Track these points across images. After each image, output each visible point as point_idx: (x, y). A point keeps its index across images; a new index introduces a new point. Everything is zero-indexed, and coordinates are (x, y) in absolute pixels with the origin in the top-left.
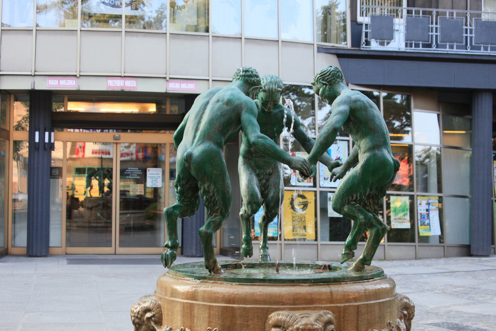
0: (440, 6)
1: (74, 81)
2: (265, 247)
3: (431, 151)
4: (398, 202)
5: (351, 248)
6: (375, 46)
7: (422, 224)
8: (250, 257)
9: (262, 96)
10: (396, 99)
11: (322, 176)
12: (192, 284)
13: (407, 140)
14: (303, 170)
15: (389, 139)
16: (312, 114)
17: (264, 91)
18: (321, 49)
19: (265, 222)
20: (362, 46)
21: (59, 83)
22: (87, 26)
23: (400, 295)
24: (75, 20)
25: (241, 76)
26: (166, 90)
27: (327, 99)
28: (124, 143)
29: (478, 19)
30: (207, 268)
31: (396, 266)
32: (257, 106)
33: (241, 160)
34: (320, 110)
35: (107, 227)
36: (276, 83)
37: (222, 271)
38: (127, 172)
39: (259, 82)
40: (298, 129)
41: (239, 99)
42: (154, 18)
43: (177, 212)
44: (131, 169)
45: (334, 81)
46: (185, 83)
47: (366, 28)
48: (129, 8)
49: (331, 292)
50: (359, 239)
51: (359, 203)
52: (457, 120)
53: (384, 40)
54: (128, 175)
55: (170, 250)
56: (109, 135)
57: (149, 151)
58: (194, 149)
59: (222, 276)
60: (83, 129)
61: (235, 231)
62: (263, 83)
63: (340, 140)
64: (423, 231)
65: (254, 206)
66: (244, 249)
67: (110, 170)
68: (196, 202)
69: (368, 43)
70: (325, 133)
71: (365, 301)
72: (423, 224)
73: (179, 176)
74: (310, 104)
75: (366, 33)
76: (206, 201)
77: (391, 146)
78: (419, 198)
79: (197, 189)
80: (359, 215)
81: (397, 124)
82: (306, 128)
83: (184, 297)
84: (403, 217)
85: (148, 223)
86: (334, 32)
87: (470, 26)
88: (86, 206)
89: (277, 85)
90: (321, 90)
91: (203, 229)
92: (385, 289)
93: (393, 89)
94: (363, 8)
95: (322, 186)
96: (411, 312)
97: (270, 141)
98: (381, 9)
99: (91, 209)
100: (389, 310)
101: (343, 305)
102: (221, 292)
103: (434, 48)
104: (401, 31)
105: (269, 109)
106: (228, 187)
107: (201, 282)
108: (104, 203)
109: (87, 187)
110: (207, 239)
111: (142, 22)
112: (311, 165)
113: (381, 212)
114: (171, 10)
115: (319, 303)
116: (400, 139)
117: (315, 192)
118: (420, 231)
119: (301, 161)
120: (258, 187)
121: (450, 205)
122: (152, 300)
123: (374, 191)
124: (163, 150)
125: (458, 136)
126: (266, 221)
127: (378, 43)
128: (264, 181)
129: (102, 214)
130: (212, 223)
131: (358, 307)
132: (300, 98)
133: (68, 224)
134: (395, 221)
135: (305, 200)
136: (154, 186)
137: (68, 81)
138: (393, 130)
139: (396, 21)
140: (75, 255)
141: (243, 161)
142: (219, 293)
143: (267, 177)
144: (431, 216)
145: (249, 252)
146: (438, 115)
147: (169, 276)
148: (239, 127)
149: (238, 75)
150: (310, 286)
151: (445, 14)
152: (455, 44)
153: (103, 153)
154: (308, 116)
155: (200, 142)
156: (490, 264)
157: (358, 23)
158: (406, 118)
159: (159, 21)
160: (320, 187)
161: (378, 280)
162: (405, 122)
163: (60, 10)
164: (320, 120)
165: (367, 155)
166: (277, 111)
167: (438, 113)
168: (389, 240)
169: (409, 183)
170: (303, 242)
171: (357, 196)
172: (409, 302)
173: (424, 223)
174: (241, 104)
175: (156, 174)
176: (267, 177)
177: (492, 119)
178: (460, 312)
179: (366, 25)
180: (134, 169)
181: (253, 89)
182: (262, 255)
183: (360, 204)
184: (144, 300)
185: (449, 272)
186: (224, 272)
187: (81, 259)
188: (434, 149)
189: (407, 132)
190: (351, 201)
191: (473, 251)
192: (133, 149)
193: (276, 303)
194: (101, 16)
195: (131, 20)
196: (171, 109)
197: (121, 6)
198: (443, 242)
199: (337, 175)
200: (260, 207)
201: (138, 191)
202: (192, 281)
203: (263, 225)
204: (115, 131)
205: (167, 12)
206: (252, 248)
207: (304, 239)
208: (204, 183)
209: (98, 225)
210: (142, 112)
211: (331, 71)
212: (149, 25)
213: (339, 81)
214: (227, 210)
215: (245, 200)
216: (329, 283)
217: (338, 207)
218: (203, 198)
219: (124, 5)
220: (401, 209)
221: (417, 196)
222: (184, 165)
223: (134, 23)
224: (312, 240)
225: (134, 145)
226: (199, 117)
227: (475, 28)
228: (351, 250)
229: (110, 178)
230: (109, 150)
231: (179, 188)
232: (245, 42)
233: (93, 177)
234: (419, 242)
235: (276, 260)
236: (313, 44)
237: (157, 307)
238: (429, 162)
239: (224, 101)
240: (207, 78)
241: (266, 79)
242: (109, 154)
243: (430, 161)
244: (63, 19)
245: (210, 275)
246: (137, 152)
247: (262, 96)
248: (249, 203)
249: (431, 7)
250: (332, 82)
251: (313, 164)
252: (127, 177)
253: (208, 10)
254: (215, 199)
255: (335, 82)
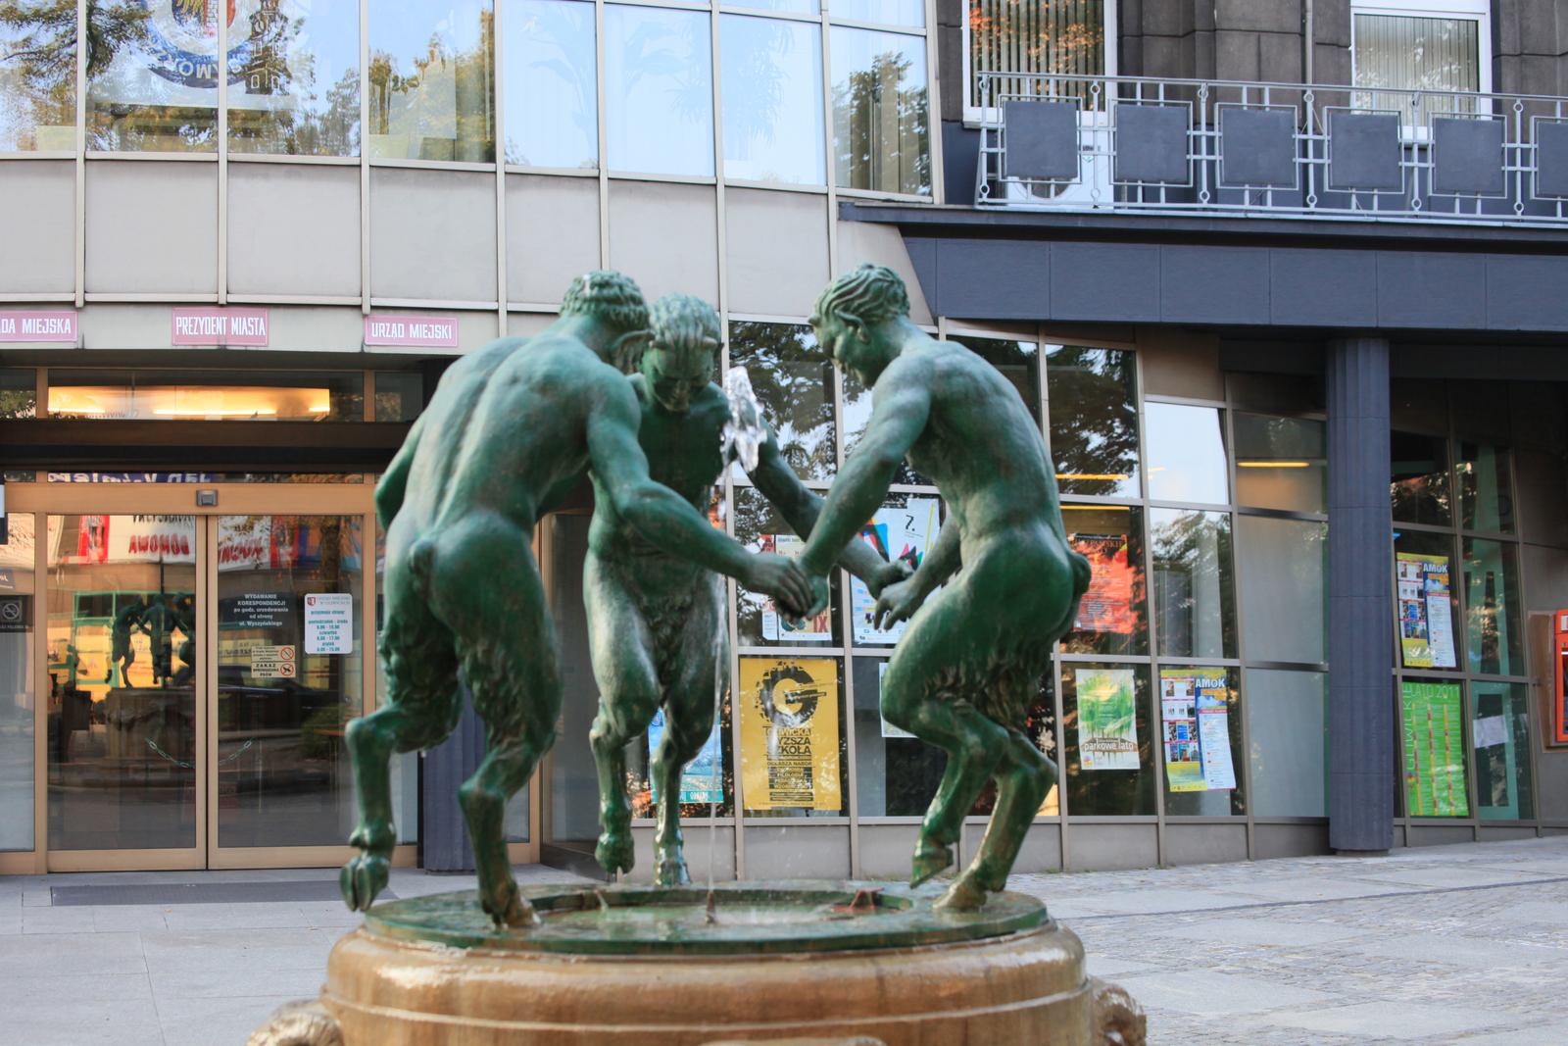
0: (1218, 75)
1: (68, 321)
2: (671, 839)
3: (1204, 522)
4: (1104, 688)
5: (941, 840)
6: (1019, 197)
7: (1410, 633)
8: (625, 871)
9: (656, 362)
10: (1092, 363)
11: (859, 609)
12: (441, 964)
13: (1126, 490)
14: (786, 595)
15: (1057, 491)
16: (829, 414)
17: (662, 346)
18: (849, 211)
19: (671, 761)
20: (980, 200)
21: (18, 326)
22: (110, 146)
23: (1101, 983)
24: (68, 129)
25: (585, 300)
26: (363, 344)
27: (860, 369)
28: (233, 515)
29: (1340, 110)
30: (487, 909)
31: (1097, 890)
32: (640, 394)
33: (591, 564)
34: (853, 403)
35: (180, 784)
36: (698, 320)
37: (536, 918)
38: (241, 607)
39: (643, 320)
40: (772, 467)
41: (581, 373)
42: (322, 118)
43: (389, 733)
44: (255, 596)
45: (880, 312)
46: (421, 322)
47: (991, 143)
48: (241, 86)
49: (881, 980)
50: (968, 809)
51: (964, 697)
52: (1280, 427)
53: (1049, 179)
54: (245, 617)
55: (370, 854)
56: (183, 491)
57: (314, 539)
58: (440, 532)
59: (534, 935)
60: (101, 472)
61: (583, 790)
62: (658, 320)
63: (915, 495)
64: (1180, 779)
65: (635, 706)
66: (606, 847)
67: (188, 601)
68: (450, 701)
69: (996, 189)
70: (852, 477)
71: (986, 1005)
72: (1180, 756)
73: (393, 619)
74: (820, 383)
75: (992, 158)
76: (481, 699)
77: (1063, 510)
78: (1164, 673)
79: (452, 661)
80: (971, 725)
81: (1096, 440)
82: (808, 459)
83: (414, 1004)
84: (1117, 736)
85: (312, 767)
86: (890, 156)
87: (1316, 131)
88: (114, 716)
89: (701, 328)
90: (840, 341)
91: (472, 785)
92: (1052, 965)
93: (1080, 332)
94: (980, 79)
95: (861, 642)
96: (1135, 1037)
97: (681, 505)
98: (1038, 82)
99: (130, 726)
100: (1063, 1032)
101: (917, 1018)
102: (531, 984)
103: (1205, 204)
104: (1099, 148)
105: (679, 402)
106: (550, 650)
107: (469, 955)
108: (170, 709)
109: (116, 658)
110: (486, 820)
111: (284, 131)
112: (810, 576)
113: (1050, 720)
114: (372, 92)
115: (844, 1015)
116: (1107, 487)
117: (840, 660)
118: (1171, 776)
119: (776, 567)
120: (647, 648)
121: (1262, 692)
122: (314, 1015)
123: (1010, 659)
124: (357, 536)
125: (1282, 480)
126: (674, 756)
127: (1029, 186)
128: (667, 631)
129: (164, 744)
130: (499, 768)
131: (966, 1023)
132: (788, 363)
133: (56, 776)
134: (1092, 747)
135: (807, 687)
136: (328, 651)
137: (47, 320)
138: (1086, 462)
139: (1086, 118)
140: (83, 876)
141: (599, 569)
142: (524, 989)
143: (675, 617)
144: (1203, 729)
145: (621, 857)
146: (1221, 412)
147: (368, 939)
148: (583, 463)
149: (576, 299)
150: (813, 959)
151: (1236, 94)
152: (1247, 187)
153: (165, 548)
154: (814, 420)
155: (458, 512)
156: (1389, 876)
157: (966, 126)
158: (1122, 423)
159: (339, 124)
160: (855, 645)
161: (1030, 936)
162: (1120, 436)
163: (21, 95)
164: (852, 434)
165: (987, 543)
166: (702, 408)
167: (1222, 405)
168: (1075, 806)
169: (1136, 627)
170: (803, 820)
171: (957, 674)
172: (1128, 1003)
173: (1414, 629)
174: (587, 389)
175: (334, 612)
176: (675, 617)
177: (1388, 421)
178: (1296, 1029)
179: (991, 132)
180: (262, 596)
181: (626, 341)
182: (663, 866)
183: (968, 698)
184: (287, 1017)
185: (1264, 905)
186: (543, 923)
187: (96, 887)
188: (1213, 517)
189: (1128, 466)
190: (939, 690)
191: (1337, 838)
192: (261, 534)
193: (714, 1016)
194: (152, 113)
195: (248, 126)
196: (375, 404)
197: (216, 80)
198: (1242, 812)
199: (897, 608)
200: (655, 712)
201: (278, 666)
202: (438, 951)
203: (665, 771)
204: (203, 476)
205: (363, 99)
206: (632, 844)
207: (808, 811)
208: (474, 642)
209: (153, 777)
210: (288, 415)
211: (870, 279)
212: (308, 140)
213: (896, 313)
214: (548, 726)
215: (606, 693)
216: (871, 951)
217: (899, 708)
218: (470, 687)
219: (223, 78)
220: (1109, 708)
221: (1161, 666)
222: (410, 585)
223: (258, 133)
224: (831, 814)
225: (266, 522)
226: (453, 431)
227: (1330, 137)
228: (942, 844)
229: (189, 627)
230: (185, 538)
231: (394, 658)
232: (611, 192)
233: (135, 626)
234: (1167, 812)
235: (705, 880)
236: (827, 195)
237: (329, 1039)
238: (1195, 559)
239: (534, 381)
240: (493, 306)
241: (668, 309)
242: (186, 550)
243: (1201, 556)
244: (29, 123)
245: (496, 933)
246: (275, 543)
247: (656, 362)
248: (621, 702)
249: (1192, 75)
250: (874, 316)
251: (819, 575)
252: (242, 624)
253: (492, 89)
254: (508, 692)
255: (882, 317)
